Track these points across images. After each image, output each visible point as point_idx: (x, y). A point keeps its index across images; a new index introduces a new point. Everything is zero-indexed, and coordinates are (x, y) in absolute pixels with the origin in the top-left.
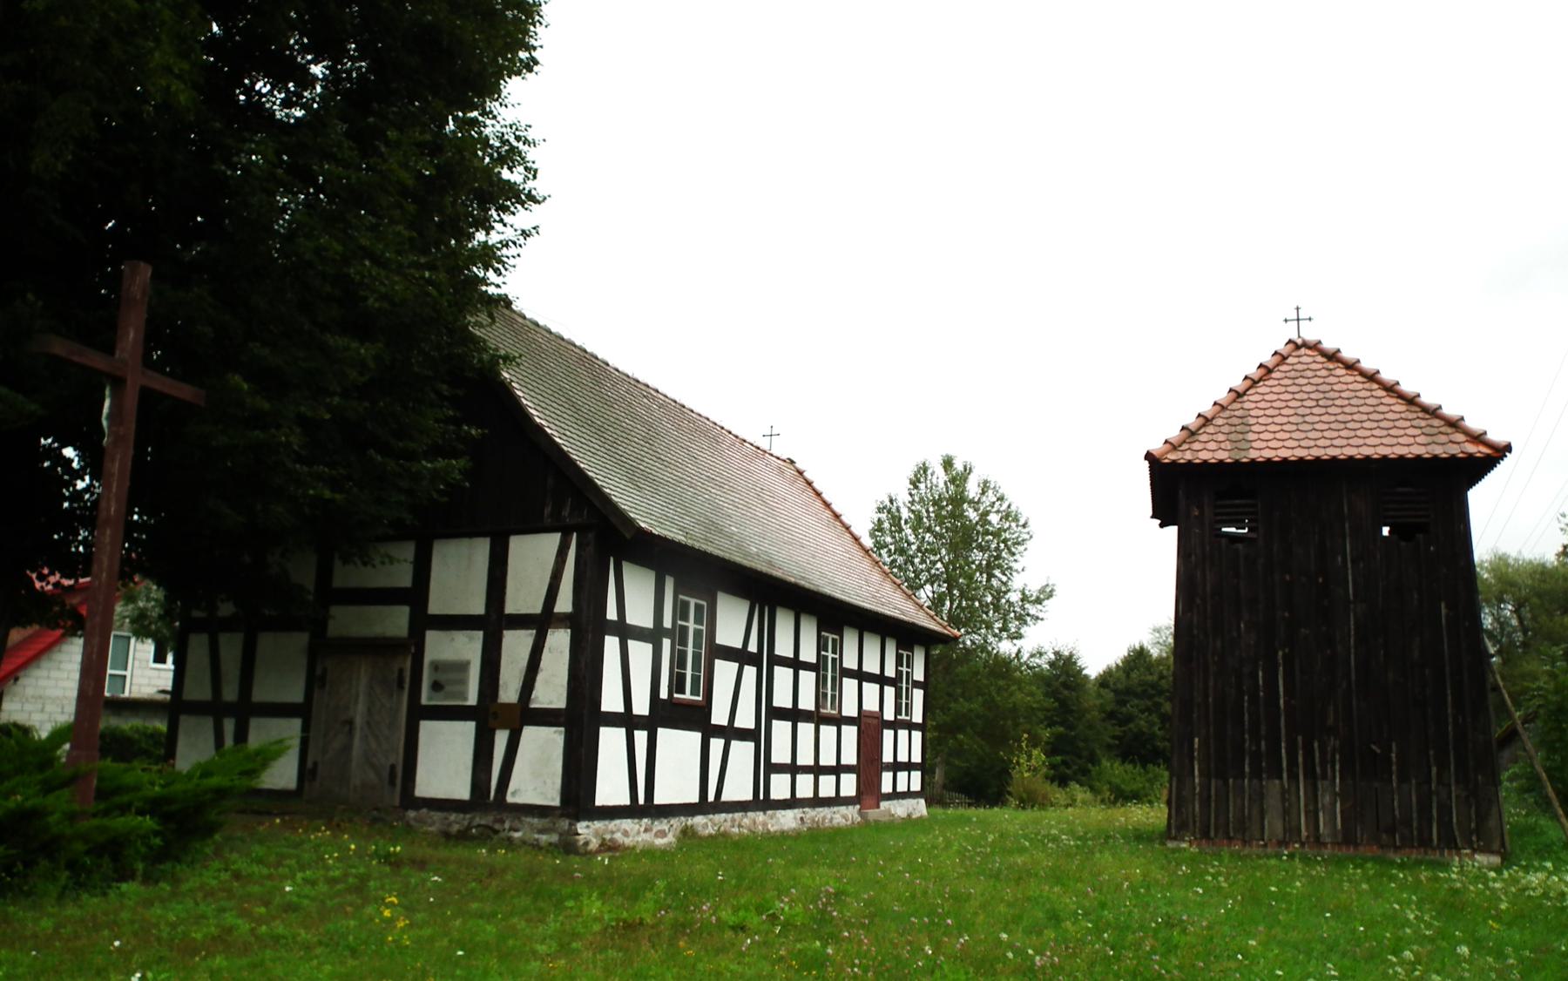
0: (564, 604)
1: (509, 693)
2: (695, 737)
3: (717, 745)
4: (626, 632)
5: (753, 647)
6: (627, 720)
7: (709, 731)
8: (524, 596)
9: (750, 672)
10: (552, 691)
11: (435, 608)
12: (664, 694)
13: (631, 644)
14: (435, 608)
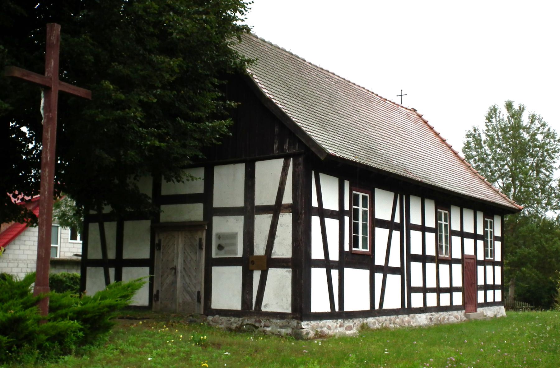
0: (288, 199)
2: (366, 273)
3: (379, 277)
4: (323, 213)
6: (327, 264)
7: (374, 269)
8: (265, 195)
9: (396, 234)
10: (283, 248)
11: (217, 204)
12: (347, 248)
14: (217, 204)
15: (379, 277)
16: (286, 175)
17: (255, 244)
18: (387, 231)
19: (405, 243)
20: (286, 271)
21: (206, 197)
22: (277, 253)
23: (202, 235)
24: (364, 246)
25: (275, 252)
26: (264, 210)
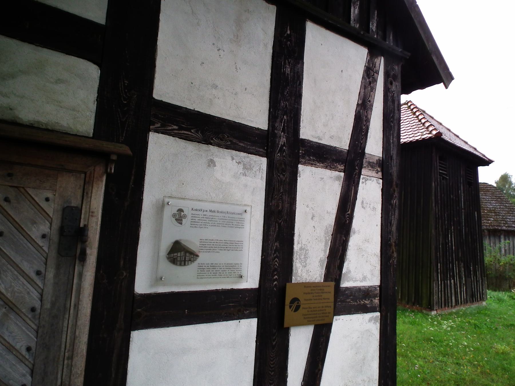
10: (183, 259)
16: (373, 89)
17: (296, 247)
20: (370, 320)
22: (353, 274)
23: (85, 194)
25: (349, 272)
26: (322, 155)
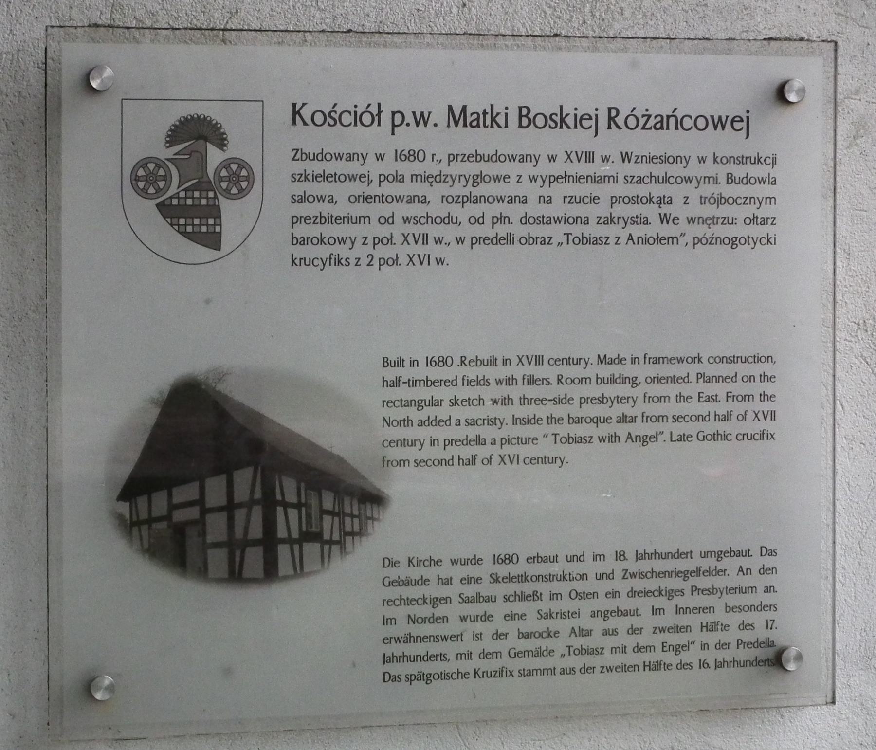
0: (258, 495)
1: (239, 533)
2: (317, 546)
3: (326, 547)
4: (286, 505)
5: (337, 510)
6: (290, 541)
7: (324, 542)
8: (241, 493)
9: (336, 519)
10: (256, 531)
11: (208, 506)
12: (304, 529)
13: (289, 510)
14: (208, 506)
15: (326, 547)
18: (330, 518)
19: (342, 524)
21: (200, 502)
24: (317, 527)
